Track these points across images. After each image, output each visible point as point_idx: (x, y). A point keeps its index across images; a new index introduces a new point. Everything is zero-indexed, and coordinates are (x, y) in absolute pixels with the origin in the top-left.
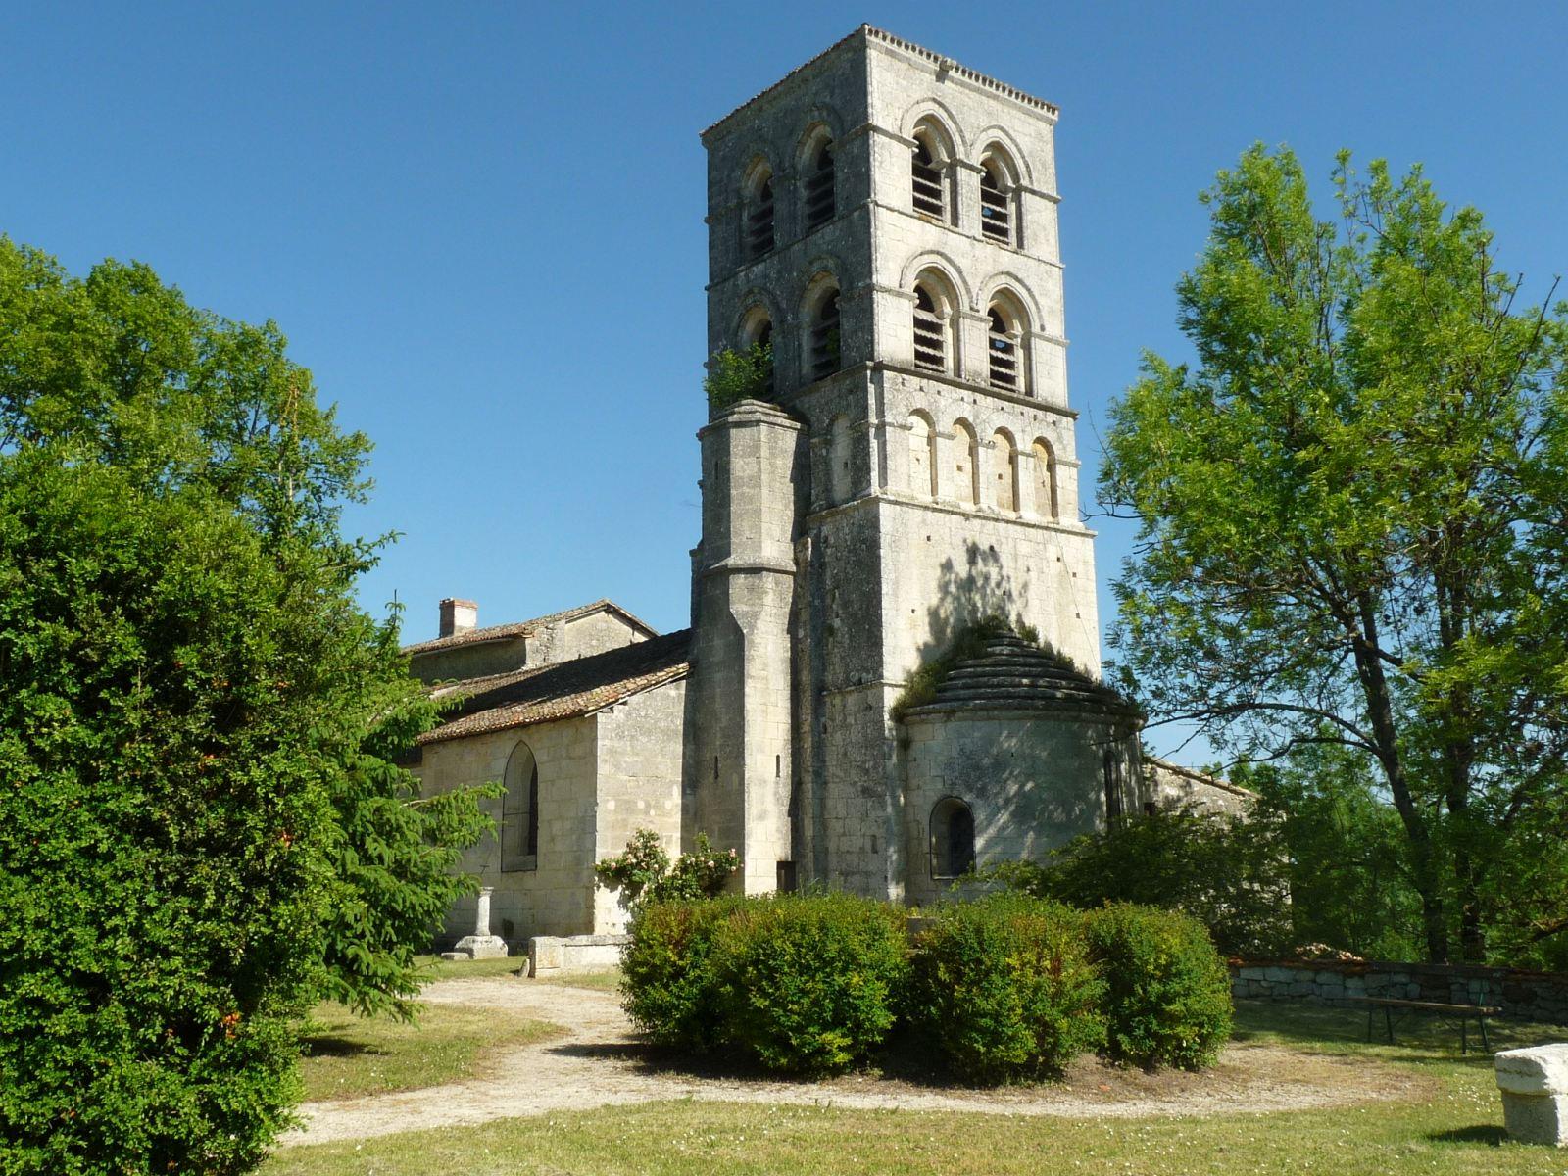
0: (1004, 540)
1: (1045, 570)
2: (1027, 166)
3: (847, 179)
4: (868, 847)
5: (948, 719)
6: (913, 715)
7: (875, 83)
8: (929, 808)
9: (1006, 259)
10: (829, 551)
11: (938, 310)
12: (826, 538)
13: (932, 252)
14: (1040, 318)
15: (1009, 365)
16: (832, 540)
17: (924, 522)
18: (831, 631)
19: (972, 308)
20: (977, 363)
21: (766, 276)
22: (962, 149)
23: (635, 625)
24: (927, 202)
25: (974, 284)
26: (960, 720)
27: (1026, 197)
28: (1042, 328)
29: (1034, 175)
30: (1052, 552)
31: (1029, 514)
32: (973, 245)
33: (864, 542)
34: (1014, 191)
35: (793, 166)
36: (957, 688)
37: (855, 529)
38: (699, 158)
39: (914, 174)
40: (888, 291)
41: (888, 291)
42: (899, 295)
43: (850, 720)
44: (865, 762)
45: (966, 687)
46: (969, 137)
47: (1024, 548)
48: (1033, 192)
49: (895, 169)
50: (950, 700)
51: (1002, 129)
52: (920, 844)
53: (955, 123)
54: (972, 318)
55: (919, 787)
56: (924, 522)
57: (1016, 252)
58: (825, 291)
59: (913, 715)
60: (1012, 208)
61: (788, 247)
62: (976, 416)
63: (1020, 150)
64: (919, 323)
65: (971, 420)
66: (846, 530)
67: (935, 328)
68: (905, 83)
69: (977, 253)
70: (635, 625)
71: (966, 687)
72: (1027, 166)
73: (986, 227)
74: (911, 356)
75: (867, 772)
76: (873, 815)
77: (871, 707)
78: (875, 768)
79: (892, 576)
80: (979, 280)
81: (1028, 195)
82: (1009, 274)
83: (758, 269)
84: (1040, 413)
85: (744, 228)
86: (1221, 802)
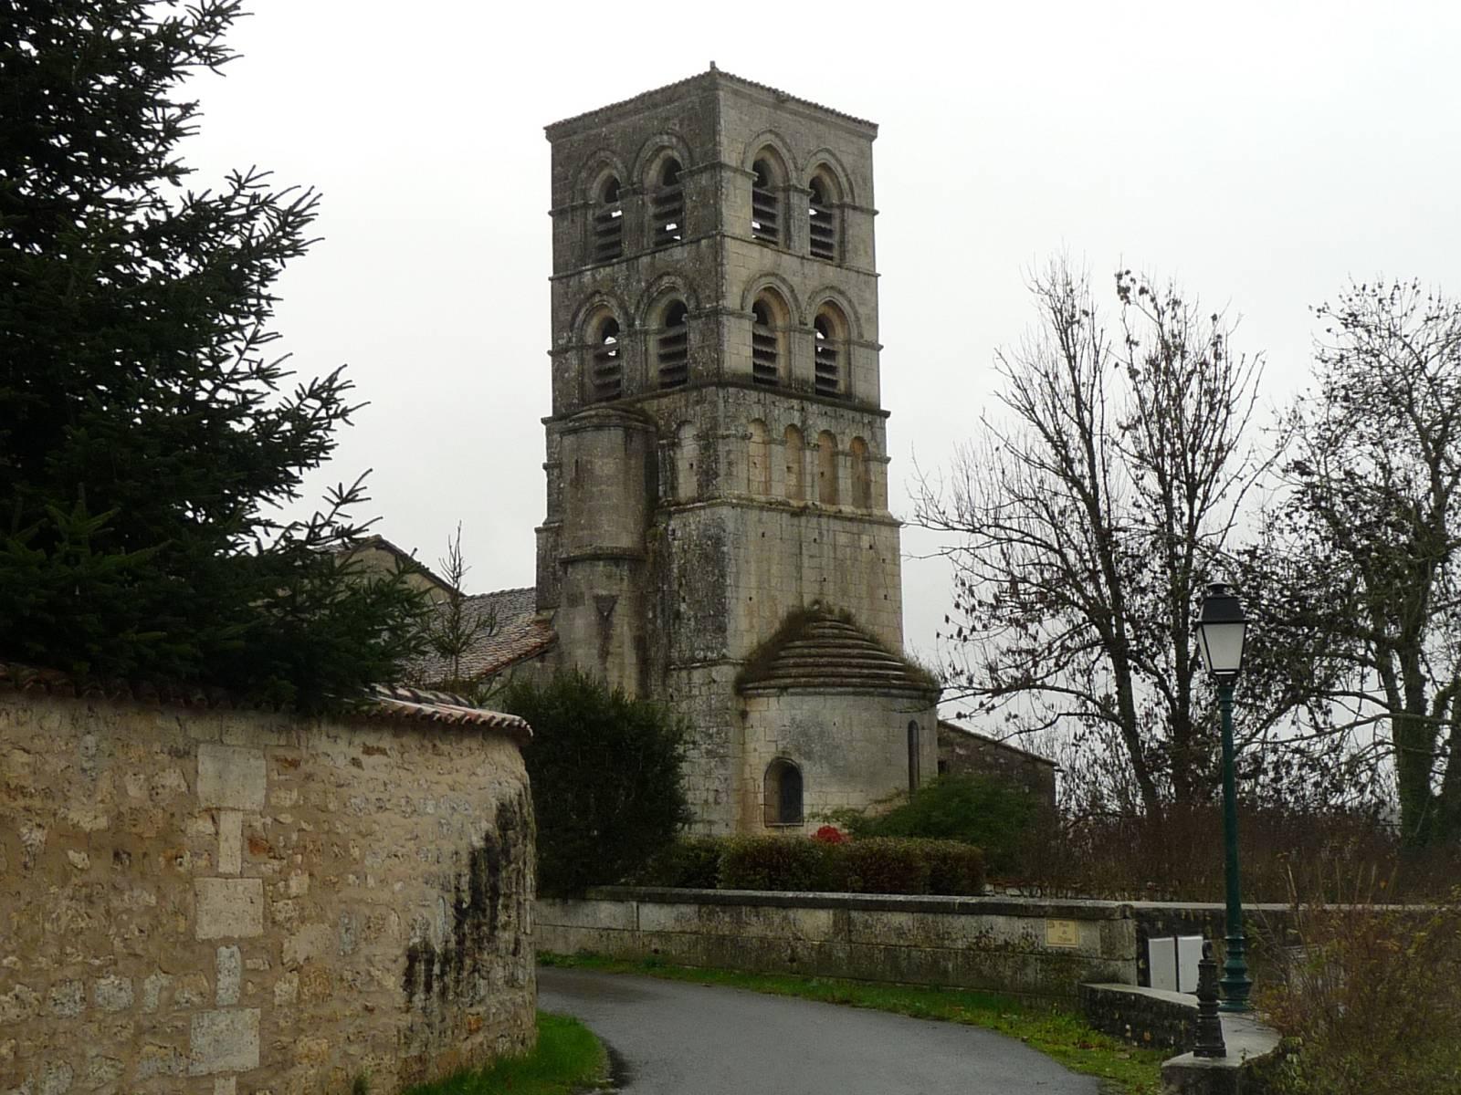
0: (825, 533)
1: (859, 558)
2: (851, 184)
3: (695, 207)
4: (711, 800)
5: (781, 694)
6: (750, 689)
7: (722, 122)
8: (764, 768)
9: (831, 273)
10: (676, 542)
11: (771, 324)
12: (674, 531)
13: (766, 275)
14: (859, 326)
15: (832, 370)
16: (679, 534)
17: (760, 521)
18: (678, 615)
19: (801, 323)
20: (805, 372)
21: (614, 280)
22: (794, 174)
23: (361, 500)
24: (766, 236)
25: (803, 299)
26: (792, 694)
27: (849, 213)
28: (861, 336)
29: (856, 191)
30: (865, 541)
31: (847, 509)
32: (802, 264)
33: (710, 538)
34: (838, 207)
35: (641, 182)
36: (788, 666)
37: (701, 527)
38: (542, 154)
39: (754, 200)
40: (731, 313)
41: (731, 313)
42: (741, 316)
43: (695, 692)
44: (708, 728)
45: (796, 665)
46: (800, 162)
47: (843, 539)
48: (855, 208)
49: (739, 200)
50: (783, 677)
51: (828, 151)
52: (756, 797)
53: (789, 151)
54: (801, 331)
55: (755, 750)
56: (760, 521)
57: (840, 266)
58: (605, 182)
59: (750, 689)
60: (836, 224)
61: (637, 258)
62: (804, 422)
63: (844, 170)
64: (757, 338)
65: (799, 425)
66: (693, 527)
67: (771, 341)
68: (747, 118)
69: (806, 271)
70: (361, 500)
71: (796, 665)
72: (851, 184)
73: (814, 243)
74: (750, 369)
75: (711, 736)
76: (716, 773)
77: (714, 681)
78: (718, 733)
79: (734, 570)
80: (806, 297)
81: (851, 211)
82: (832, 288)
83: (604, 272)
84: (858, 416)
85: (590, 228)
86: (1002, 761)
